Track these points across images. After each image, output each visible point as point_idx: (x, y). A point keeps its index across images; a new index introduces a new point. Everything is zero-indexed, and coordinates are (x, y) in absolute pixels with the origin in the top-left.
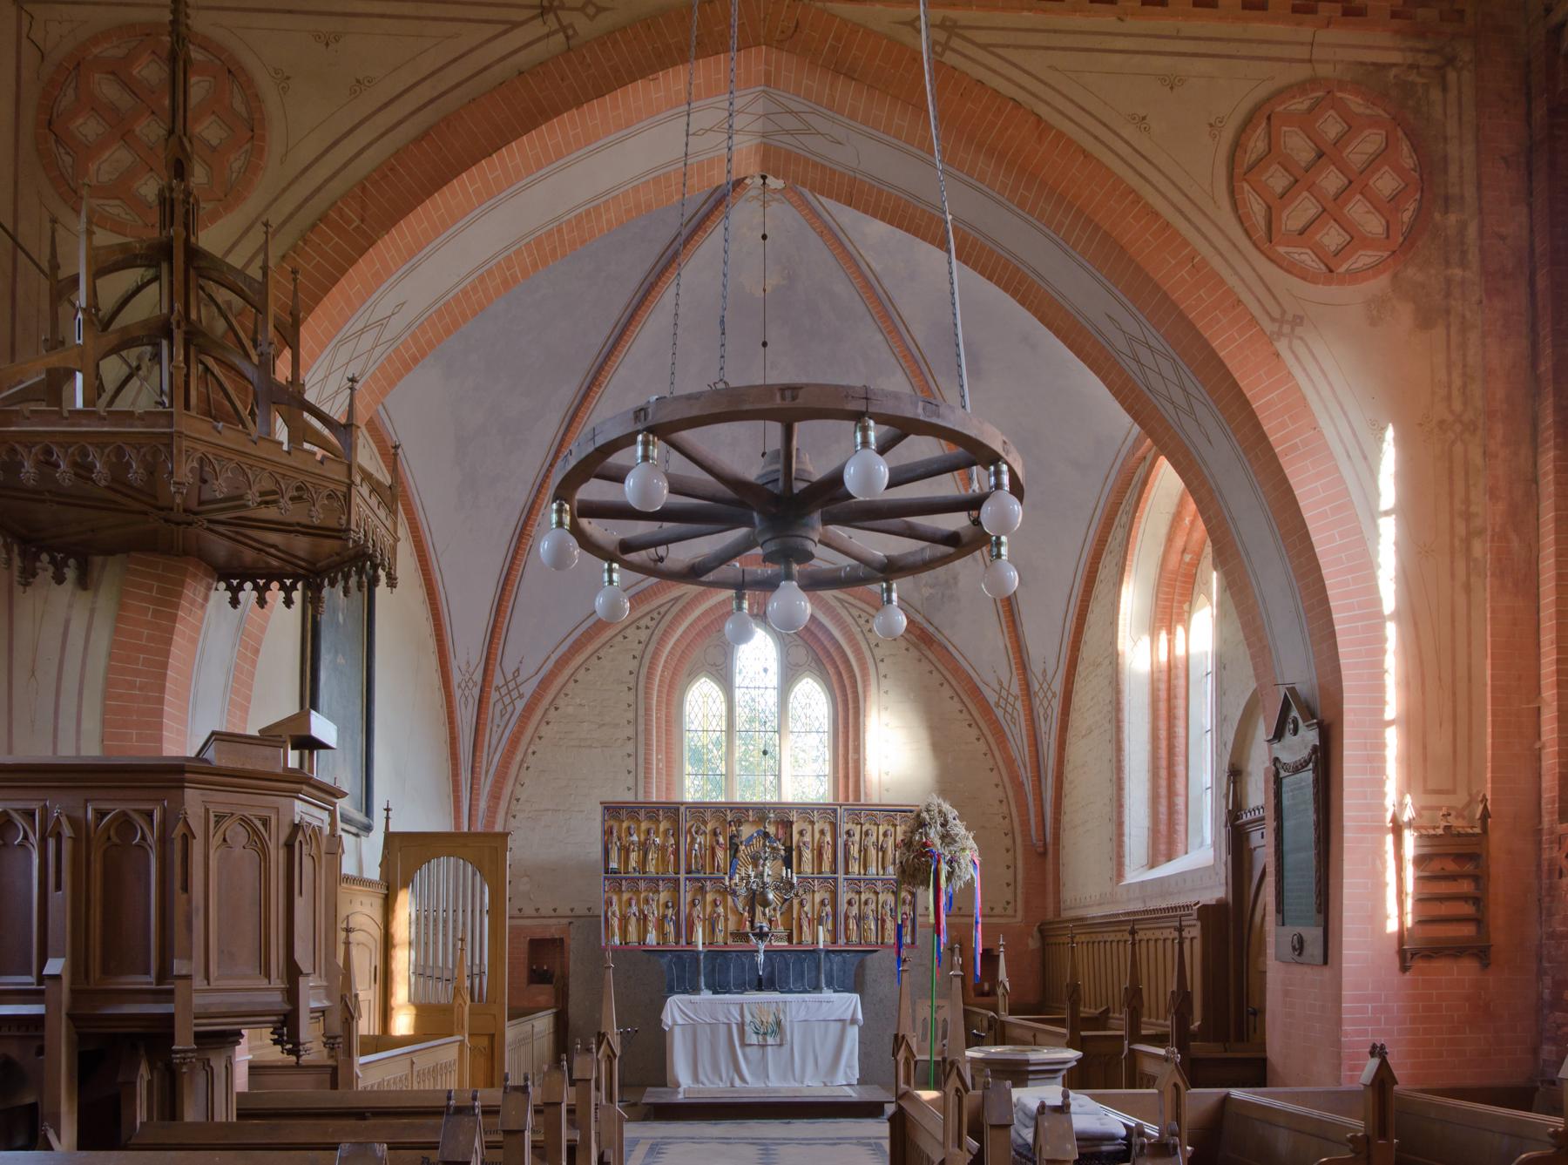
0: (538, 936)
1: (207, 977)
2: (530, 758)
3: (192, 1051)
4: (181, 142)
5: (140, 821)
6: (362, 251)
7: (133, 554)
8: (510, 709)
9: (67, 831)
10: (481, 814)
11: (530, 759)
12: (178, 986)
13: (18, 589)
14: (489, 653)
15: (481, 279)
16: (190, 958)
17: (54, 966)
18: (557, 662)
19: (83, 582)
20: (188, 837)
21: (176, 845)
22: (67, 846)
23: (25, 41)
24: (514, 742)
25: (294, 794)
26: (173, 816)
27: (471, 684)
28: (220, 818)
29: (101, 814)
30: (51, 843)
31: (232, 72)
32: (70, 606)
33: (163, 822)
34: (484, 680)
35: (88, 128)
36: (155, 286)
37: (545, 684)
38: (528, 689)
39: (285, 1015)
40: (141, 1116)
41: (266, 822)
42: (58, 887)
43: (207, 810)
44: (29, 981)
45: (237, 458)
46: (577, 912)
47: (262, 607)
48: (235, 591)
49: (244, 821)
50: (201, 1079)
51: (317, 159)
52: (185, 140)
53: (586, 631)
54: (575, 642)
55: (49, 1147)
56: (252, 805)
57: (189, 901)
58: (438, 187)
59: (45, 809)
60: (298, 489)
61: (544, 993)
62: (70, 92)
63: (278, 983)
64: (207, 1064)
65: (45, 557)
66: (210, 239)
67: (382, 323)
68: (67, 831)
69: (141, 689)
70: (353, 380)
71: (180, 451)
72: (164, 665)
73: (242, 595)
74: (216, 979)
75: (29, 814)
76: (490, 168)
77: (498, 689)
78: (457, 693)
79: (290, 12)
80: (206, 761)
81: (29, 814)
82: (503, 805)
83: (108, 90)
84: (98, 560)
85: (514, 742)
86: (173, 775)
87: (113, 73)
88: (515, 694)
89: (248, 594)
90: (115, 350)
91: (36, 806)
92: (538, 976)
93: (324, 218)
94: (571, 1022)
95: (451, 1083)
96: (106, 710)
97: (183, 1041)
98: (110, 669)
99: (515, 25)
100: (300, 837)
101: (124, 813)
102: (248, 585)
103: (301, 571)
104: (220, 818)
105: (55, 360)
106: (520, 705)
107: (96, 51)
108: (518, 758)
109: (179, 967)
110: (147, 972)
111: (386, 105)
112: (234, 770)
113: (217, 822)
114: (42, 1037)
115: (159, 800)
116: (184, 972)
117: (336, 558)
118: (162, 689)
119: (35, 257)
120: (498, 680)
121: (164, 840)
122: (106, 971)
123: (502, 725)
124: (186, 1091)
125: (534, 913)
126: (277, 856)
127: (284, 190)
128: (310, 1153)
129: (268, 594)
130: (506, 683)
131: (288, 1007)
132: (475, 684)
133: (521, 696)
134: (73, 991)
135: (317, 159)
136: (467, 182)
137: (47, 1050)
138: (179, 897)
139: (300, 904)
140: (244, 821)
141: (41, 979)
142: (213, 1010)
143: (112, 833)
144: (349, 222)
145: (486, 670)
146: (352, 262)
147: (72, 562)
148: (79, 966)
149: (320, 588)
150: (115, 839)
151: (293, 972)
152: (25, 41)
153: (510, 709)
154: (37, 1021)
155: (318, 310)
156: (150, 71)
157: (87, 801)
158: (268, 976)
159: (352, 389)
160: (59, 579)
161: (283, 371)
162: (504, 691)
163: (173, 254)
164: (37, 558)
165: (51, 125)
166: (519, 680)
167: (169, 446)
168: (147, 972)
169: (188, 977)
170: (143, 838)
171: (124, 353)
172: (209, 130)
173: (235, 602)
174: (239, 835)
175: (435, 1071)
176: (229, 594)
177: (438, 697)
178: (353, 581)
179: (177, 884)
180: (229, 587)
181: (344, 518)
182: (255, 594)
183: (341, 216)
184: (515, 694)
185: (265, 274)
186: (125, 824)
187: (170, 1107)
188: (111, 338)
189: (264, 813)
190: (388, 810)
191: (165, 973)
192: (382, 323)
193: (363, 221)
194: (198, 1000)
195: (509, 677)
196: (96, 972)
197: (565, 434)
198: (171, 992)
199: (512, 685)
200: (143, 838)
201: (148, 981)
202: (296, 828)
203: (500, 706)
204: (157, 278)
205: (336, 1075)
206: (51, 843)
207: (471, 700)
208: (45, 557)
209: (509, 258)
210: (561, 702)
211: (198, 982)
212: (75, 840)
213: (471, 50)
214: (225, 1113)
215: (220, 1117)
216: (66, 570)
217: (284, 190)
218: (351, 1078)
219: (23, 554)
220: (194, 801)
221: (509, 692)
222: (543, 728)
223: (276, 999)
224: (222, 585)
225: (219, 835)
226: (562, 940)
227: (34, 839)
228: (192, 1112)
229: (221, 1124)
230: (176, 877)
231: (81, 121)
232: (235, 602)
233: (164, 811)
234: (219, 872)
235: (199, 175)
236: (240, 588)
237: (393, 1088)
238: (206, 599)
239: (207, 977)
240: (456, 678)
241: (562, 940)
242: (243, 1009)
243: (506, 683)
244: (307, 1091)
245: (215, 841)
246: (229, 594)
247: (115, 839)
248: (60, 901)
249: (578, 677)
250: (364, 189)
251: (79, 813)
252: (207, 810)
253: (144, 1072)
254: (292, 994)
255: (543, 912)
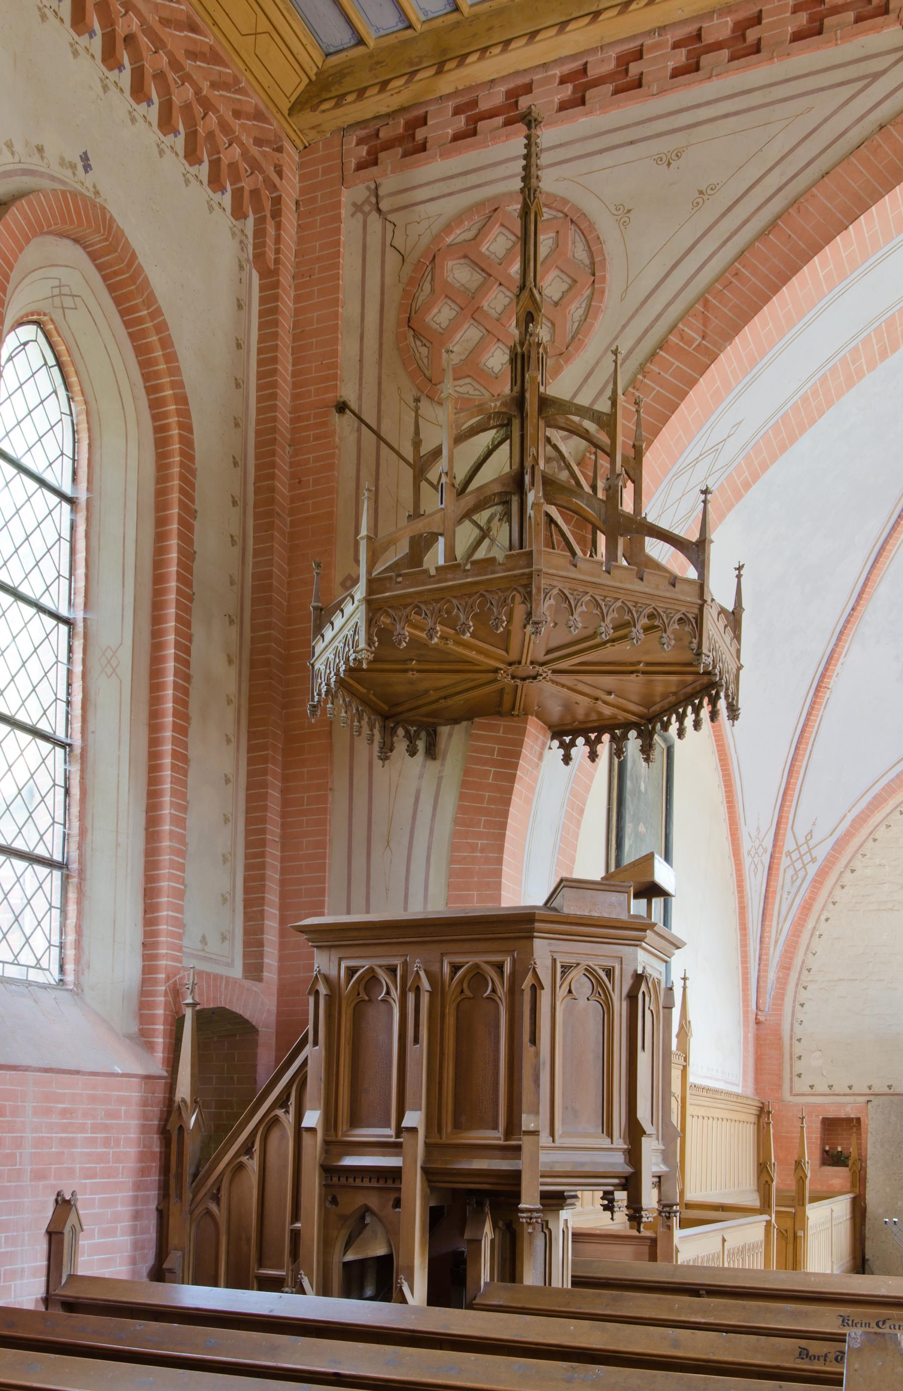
0: (831, 1115)
1: (552, 1134)
2: (823, 925)
3: (537, 1211)
4: (532, 295)
5: (491, 973)
6: (703, 369)
7: (476, 720)
8: (801, 874)
9: (425, 985)
10: (769, 986)
11: (823, 927)
12: (526, 1142)
13: (378, 763)
14: (780, 817)
15: (824, 380)
16: (537, 1113)
17: (414, 1118)
18: (854, 821)
19: (431, 752)
20: (536, 988)
21: (523, 994)
22: (425, 999)
23: (388, 249)
24: (806, 908)
25: (636, 942)
26: (524, 966)
27: (760, 851)
28: (566, 968)
29: (455, 968)
30: (411, 997)
31: (576, 220)
32: (421, 777)
33: (513, 973)
34: (774, 846)
35: (442, 315)
36: (506, 446)
37: (839, 846)
38: (821, 852)
39: (626, 1178)
40: (485, 1276)
41: (609, 972)
42: (416, 1040)
43: (554, 961)
44: (388, 1133)
45: (591, 591)
46: (876, 1090)
47: (593, 760)
48: (567, 748)
49: (589, 972)
50: (539, 1241)
51: (658, 286)
52: (535, 292)
53: (888, 785)
54: (875, 798)
55: (404, 1301)
56: (598, 955)
57: (537, 1054)
58: (785, 279)
59: (405, 964)
60: (651, 616)
61: (838, 1176)
62: (427, 287)
63: (620, 1143)
64: (545, 1225)
65: (401, 732)
66: (561, 385)
67: (716, 449)
68: (425, 985)
69: (482, 851)
70: (705, 492)
71: (539, 589)
72: (503, 826)
73: (573, 751)
74: (563, 1139)
75: (392, 970)
76: (842, 245)
77: (789, 854)
78: (747, 861)
79: (632, 143)
80: (555, 909)
81: (392, 970)
82: (794, 975)
83: (459, 274)
84: (444, 730)
85: (806, 908)
86: (519, 926)
87: (465, 257)
88: (807, 859)
89: (580, 749)
90: (468, 515)
91: (397, 962)
92: (832, 1158)
93: (662, 345)
94: (869, 1209)
95: (757, 1263)
96: (452, 874)
97: (529, 1201)
98: (455, 834)
99: (876, 76)
100: (643, 988)
101: (476, 966)
102: (580, 741)
103: (634, 719)
104: (566, 968)
105: (420, 526)
106: (812, 869)
107: (449, 240)
108: (810, 925)
109: (528, 1122)
110: (495, 1127)
111: (729, 209)
112: (582, 917)
113: (563, 973)
114: (399, 1189)
115: (510, 952)
116: (532, 1127)
117: (672, 699)
118: (501, 849)
119: (396, 446)
120: (789, 844)
121: (514, 991)
122: (457, 1126)
123: (793, 891)
124: (525, 1253)
125: (827, 1091)
126: (620, 1008)
127: (624, 327)
128: (670, 1331)
129: (599, 747)
130: (798, 848)
131: (629, 1170)
132: (765, 851)
133: (813, 860)
134: (427, 1145)
135: (658, 286)
136: (818, 267)
137: (403, 1202)
138: (528, 1050)
139: (643, 1059)
140: (589, 972)
141: (399, 1131)
142: (558, 1168)
143: (465, 985)
144: (689, 342)
145: (776, 834)
146: (692, 383)
147: (423, 734)
148: (433, 1122)
149: (651, 734)
150: (467, 992)
151: (635, 1132)
152: (388, 249)
153: (801, 874)
154: (395, 1174)
155: (656, 443)
156: (499, 243)
157: (442, 955)
158: (610, 1135)
159: (705, 502)
160: (412, 752)
161: (628, 506)
162: (795, 856)
163: (522, 411)
164: (393, 732)
165: (412, 322)
166: (812, 843)
167: (528, 586)
168: (495, 1127)
169: (535, 1133)
170: (494, 991)
171: (475, 518)
172: (551, 285)
173: (567, 759)
174: (582, 986)
175: (742, 1251)
176: (562, 752)
177: (729, 865)
178: (705, 713)
179: (526, 1037)
180: (562, 745)
181: (695, 641)
182: (587, 749)
183: (682, 339)
184: (807, 859)
185: (614, 404)
186: (477, 977)
187: (509, 1268)
188: (468, 500)
189: (608, 963)
190: (685, 979)
191: (513, 1128)
192: (716, 449)
193: (704, 338)
194: (546, 1159)
195: (801, 840)
196: (448, 1127)
197: (870, 572)
198: (518, 1148)
199: (804, 849)
200: (494, 991)
201: (495, 1137)
202: (639, 978)
203: (790, 872)
204: (508, 437)
205: (654, 1248)
206: (411, 997)
207: (760, 867)
208: (401, 732)
209: (856, 349)
210: (857, 864)
211: (544, 1139)
212: (432, 994)
213: (826, 120)
214: (561, 1279)
215: (556, 1283)
216: (418, 742)
217: (624, 327)
218: (671, 1253)
219: (384, 728)
220: (543, 951)
221: (801, 857)
222: (838, 892)
223: (617, 1161)
224: (556, 743)
225: (565, 987)
226: (858, 1120)
227: (395, 994)
228: (531, 1276)
229: (557, 1289)
230: (523, 1030)
231: (435, 310)
232: (567, 759)
233: (514, 962)
234: (568, 1024)
235: (543, 333)
236: (573, 744)
237: (711, 1264)
238: (541, 757)
239: (552, 1134)
240: (746, 844)
241: (858, 1120)
242: (587, 1169)
243: (798, 848)
244: (626, 1262)
245: (561, 992)
246: (562, 752)
247: (467, 992)
248: (418, 1054)
249: (878, 835)
250: (706, 301)
251: (435, 968)
252: (554, 961)
253: (488, 1228)
254: (634, 1155)
255: (836, 1089)
